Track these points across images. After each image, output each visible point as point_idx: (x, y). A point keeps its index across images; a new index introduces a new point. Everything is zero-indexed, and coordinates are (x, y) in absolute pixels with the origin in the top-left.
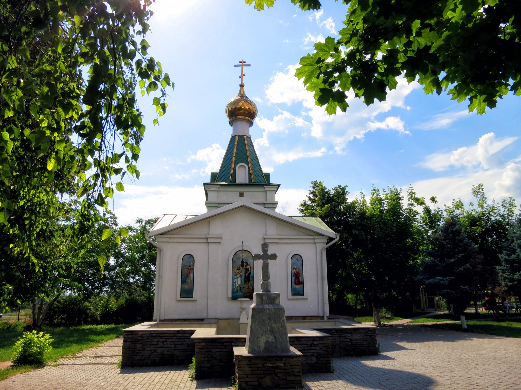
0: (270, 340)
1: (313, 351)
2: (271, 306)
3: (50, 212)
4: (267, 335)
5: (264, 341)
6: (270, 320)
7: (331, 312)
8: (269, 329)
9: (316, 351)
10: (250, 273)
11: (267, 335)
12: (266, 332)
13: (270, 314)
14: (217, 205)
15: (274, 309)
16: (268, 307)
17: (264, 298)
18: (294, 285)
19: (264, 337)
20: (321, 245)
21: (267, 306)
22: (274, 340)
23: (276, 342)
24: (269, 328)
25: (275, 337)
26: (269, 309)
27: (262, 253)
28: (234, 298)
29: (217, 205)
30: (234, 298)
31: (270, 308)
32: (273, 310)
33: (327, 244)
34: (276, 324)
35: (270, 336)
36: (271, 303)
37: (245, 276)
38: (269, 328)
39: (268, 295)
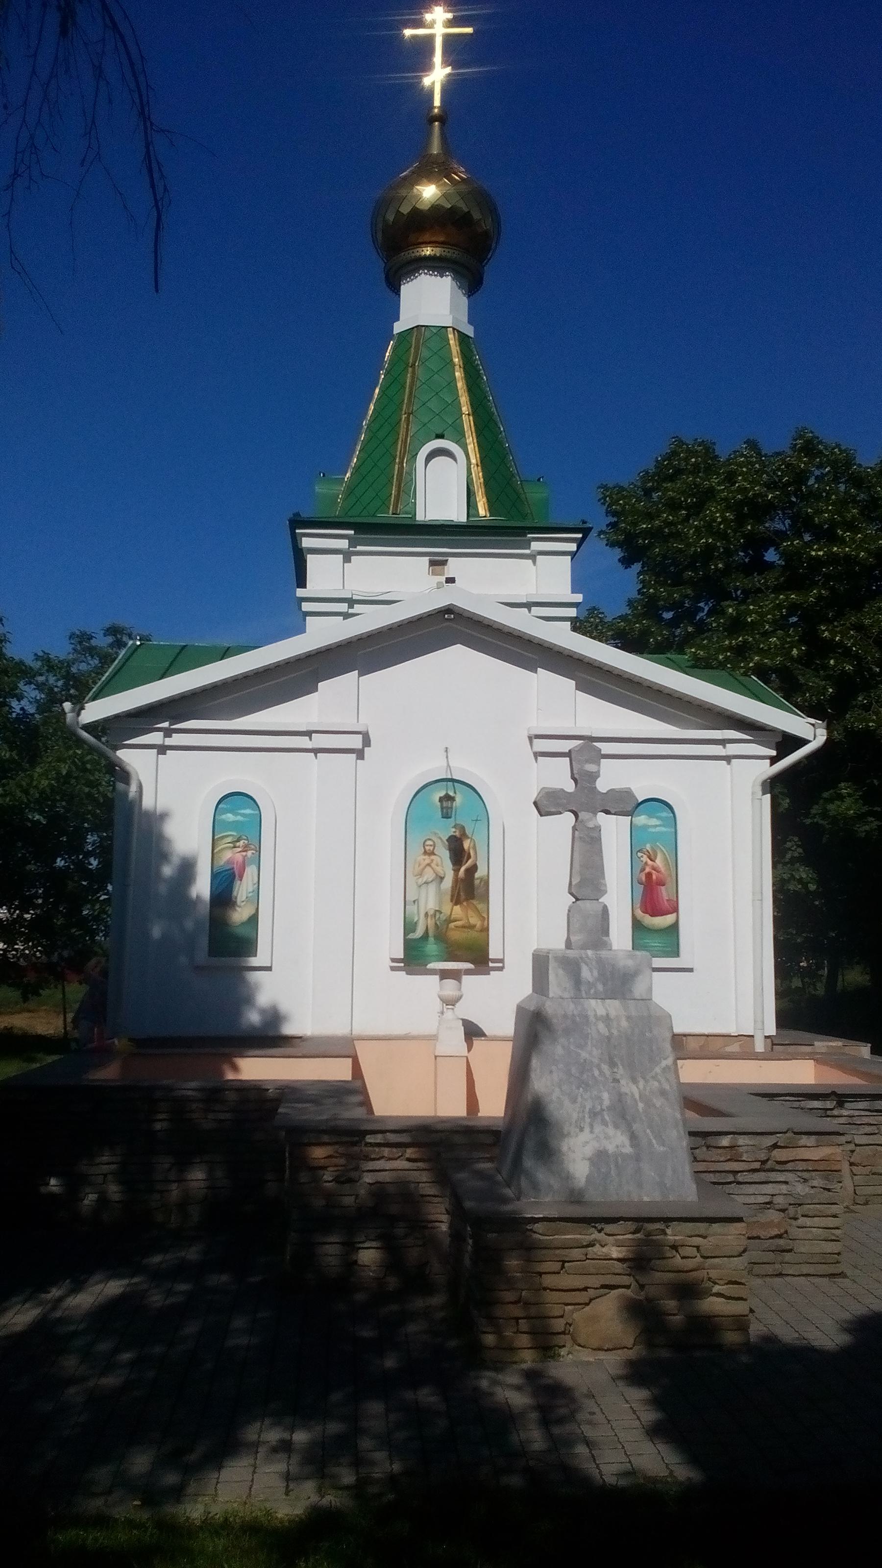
0: (611, 1148)
1: (769, 1189)
2: (613, 1007)
3: (507, 1418)
4: (598, 1129)
5: (589, 1151)
6: (612, 1064)
7: (784, 1019)
8: (606, 1103)
9: (784, 1188)
10: (474, 869)
11: (598, 1129)
12: (594, 1114)
13: (609, 1038)
14: (343, 607)
15: (629, 1018)
16: (601, 1012)
17: (586, 974)
18: (639, 913)
19: (585, 1136)
20: (757, 767)
21: (596, 1007)
22: (628, 1150)
23: (638, 1158)
24: (605, 1095)
25: (633, 1138)
26: (607, 1019)
27: (569, 786)
28: (413, 959)
29: (343, 607)
30: (413, 959)
31: (613, 1014)
32: (624, 1023)
33: (774, 760)
34: (634, 1080)
35: (611, 1131)
36: (610, 994)
37: (456, 880)
38: (605, 1095)
39: (600, 961)
